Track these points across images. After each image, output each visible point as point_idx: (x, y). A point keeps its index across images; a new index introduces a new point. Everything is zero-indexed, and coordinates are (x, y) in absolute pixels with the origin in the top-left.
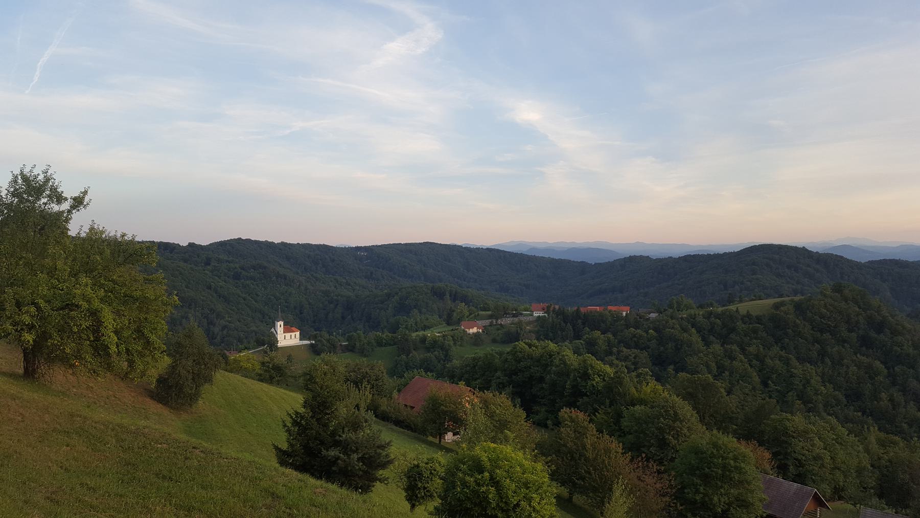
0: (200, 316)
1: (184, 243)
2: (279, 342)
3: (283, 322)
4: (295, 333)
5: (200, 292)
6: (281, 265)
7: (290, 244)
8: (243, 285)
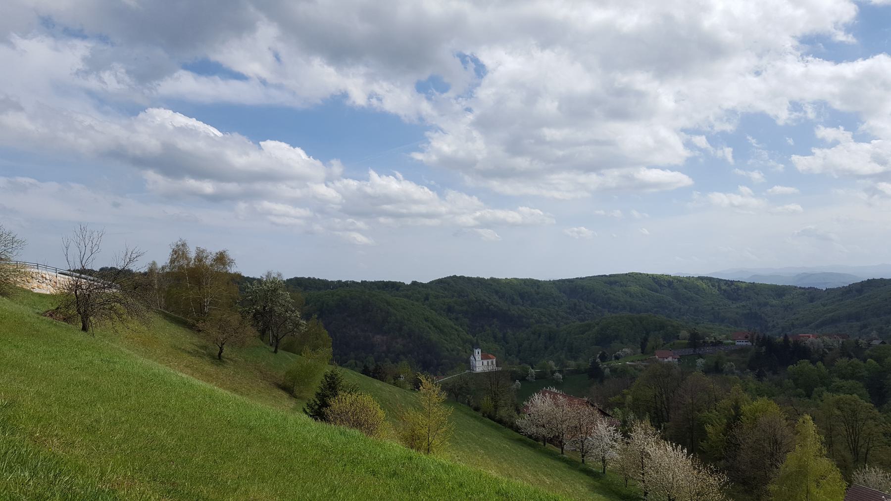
1: (408, 282)
2: (477, 368)
3: (480, 350)
4: (491, 360)
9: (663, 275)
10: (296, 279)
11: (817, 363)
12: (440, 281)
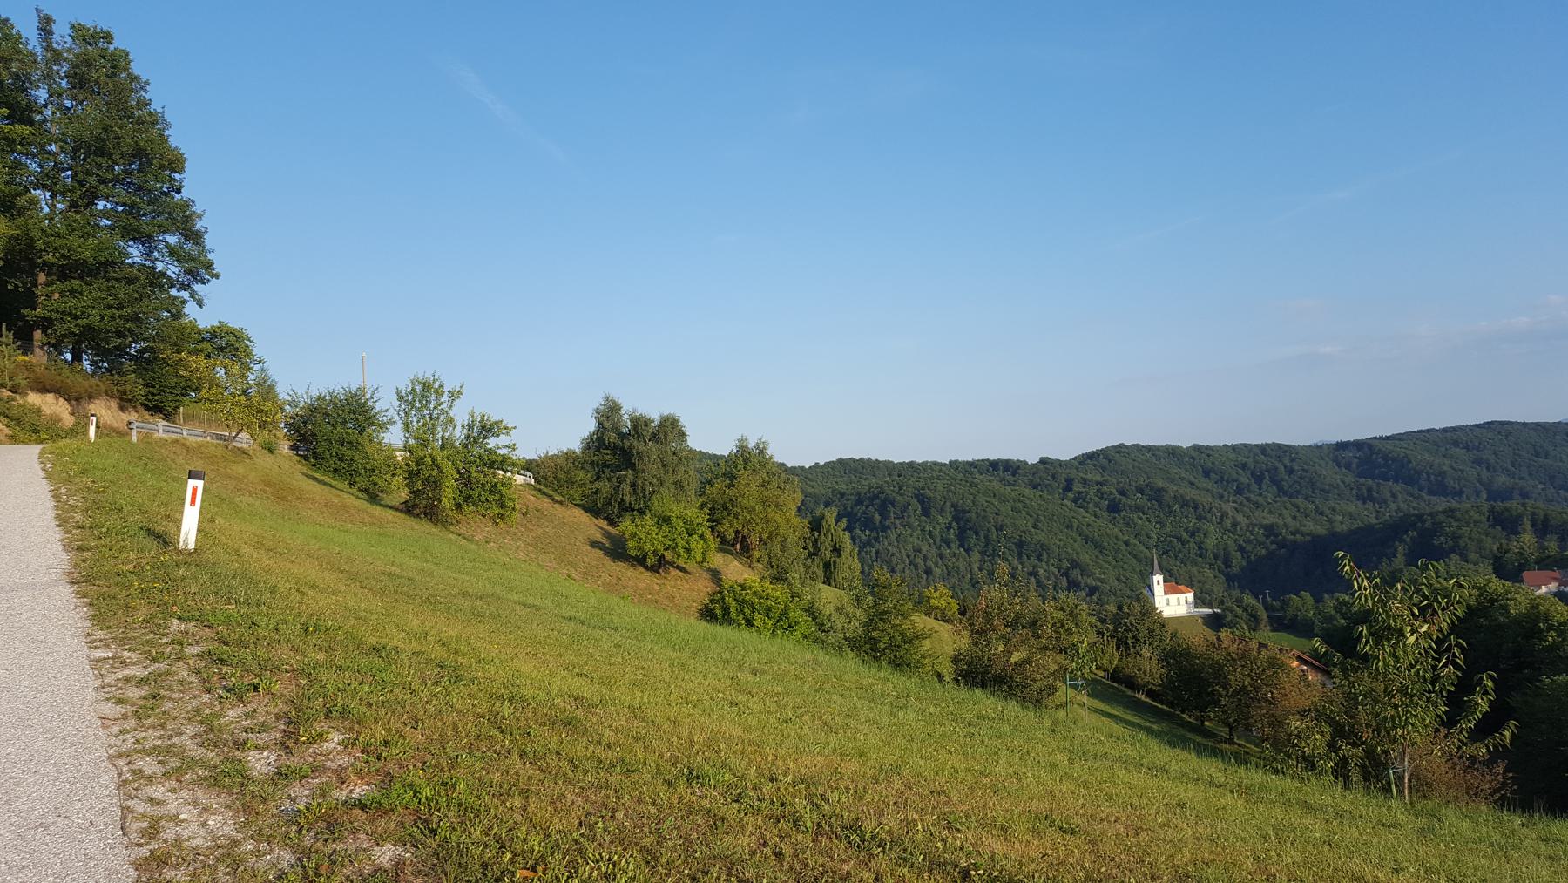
0: (1057, 573)
1: (1033, 459)
5: (1056, 534)
6: (1192, 484)
7: (1208, 448)
8: (1124, 520)
10: (841, 461)
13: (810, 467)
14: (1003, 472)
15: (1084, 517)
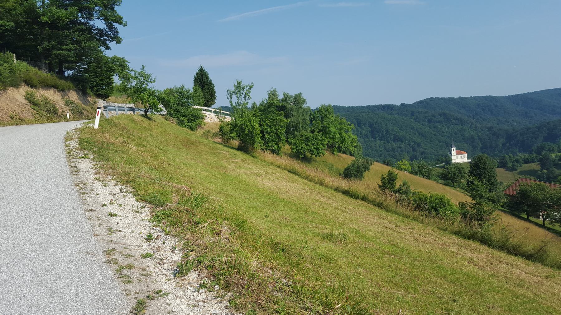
1: (398, 104)
3: (455, 148)
9: (21, 124)
11: (527, 216)
12: (421, 102)
13: (315, 109)
14: (387, 109)
15: (419, 125)
